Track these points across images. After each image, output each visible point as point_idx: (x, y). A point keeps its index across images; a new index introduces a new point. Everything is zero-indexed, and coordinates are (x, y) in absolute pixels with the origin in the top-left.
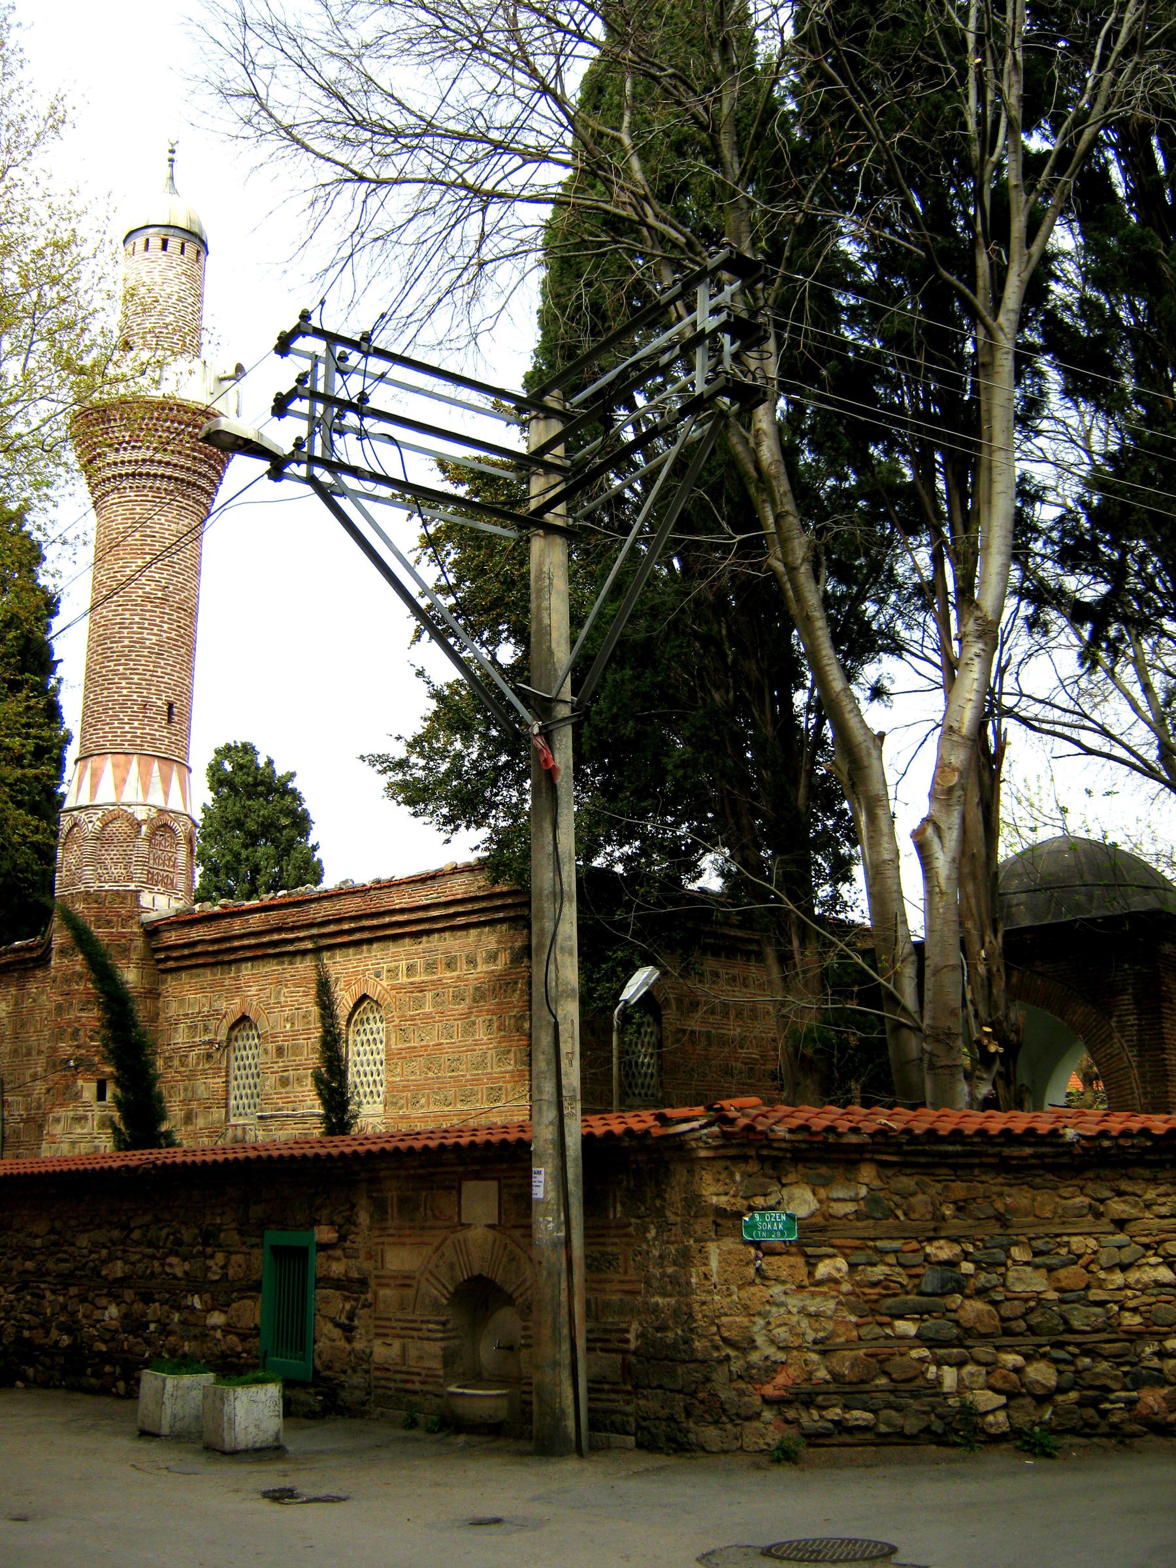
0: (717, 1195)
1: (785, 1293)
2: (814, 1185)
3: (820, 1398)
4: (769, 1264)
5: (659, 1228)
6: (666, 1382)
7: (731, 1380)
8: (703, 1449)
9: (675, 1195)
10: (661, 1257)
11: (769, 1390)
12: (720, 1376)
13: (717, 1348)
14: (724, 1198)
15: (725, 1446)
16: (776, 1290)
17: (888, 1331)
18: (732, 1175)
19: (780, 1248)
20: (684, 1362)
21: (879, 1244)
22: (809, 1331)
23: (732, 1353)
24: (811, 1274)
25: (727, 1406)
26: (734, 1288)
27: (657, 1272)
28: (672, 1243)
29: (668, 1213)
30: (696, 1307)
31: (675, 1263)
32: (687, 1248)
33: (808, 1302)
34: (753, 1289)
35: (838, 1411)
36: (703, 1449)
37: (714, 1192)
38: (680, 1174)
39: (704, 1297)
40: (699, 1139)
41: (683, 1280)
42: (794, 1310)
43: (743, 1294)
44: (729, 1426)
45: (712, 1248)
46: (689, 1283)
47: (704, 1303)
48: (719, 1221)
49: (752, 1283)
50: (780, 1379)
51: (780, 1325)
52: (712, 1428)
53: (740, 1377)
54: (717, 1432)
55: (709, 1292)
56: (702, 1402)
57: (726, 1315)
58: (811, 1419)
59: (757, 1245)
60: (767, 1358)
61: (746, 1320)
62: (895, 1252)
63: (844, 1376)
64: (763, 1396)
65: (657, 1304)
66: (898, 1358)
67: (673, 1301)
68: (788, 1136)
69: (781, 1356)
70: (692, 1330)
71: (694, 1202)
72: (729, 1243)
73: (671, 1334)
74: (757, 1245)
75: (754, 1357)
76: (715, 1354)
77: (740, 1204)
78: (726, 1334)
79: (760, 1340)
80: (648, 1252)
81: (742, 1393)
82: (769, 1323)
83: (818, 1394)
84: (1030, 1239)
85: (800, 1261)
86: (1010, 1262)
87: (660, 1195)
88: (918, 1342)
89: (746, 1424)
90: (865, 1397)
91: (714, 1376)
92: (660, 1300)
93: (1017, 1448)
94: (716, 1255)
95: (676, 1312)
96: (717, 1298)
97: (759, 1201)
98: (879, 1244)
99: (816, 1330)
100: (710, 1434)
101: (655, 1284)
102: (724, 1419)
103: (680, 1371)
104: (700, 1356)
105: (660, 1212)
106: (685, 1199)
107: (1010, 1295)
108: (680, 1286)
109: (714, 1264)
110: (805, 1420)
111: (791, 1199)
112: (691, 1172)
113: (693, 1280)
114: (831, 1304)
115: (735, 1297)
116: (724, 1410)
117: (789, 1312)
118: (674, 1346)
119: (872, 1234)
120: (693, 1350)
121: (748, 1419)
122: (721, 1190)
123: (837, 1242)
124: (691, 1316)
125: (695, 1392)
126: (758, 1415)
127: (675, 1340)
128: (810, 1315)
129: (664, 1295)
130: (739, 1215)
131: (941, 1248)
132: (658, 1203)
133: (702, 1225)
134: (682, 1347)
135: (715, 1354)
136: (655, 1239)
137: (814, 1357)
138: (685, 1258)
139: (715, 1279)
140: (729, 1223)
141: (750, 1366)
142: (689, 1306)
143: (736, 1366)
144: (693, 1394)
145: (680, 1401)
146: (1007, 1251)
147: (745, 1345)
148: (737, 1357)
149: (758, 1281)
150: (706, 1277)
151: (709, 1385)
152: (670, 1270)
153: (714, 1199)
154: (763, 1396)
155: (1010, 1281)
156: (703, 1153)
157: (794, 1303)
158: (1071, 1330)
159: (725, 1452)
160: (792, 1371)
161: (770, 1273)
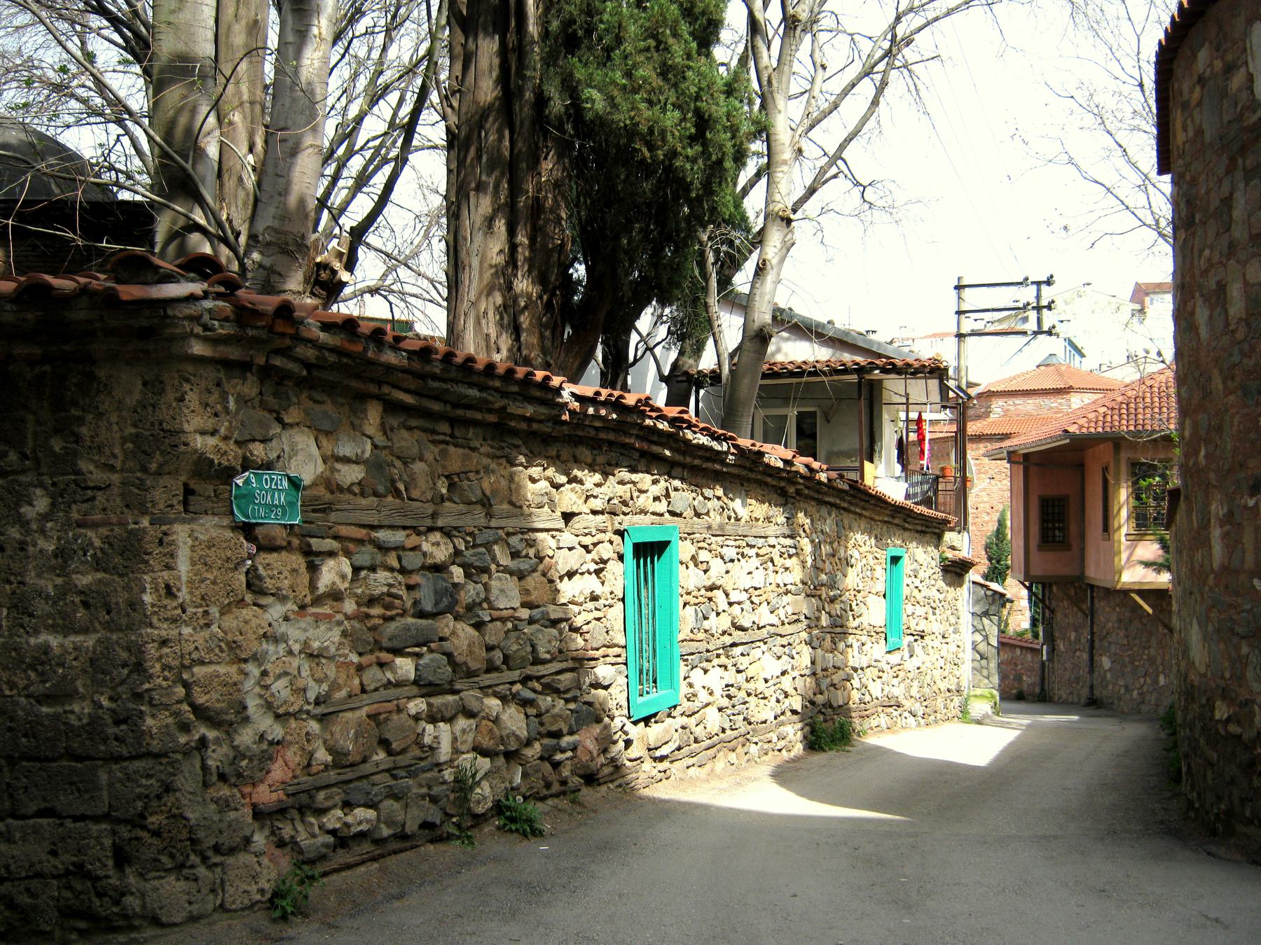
0: (203, 433)
1: (286, 619)
2: (322, 432)
3: (321, 795)
4: (267, 566)
5: (59, 497)
6: (65, 801)
7: (206, 785)
8: (156, 922)
9: (110, 429)
10: (60, 553)
11: (265, 795)
12: (187, 779)
13: (185, 728)
14: (212, 441)
15: (195, 908)
16: (276, 611)
17: (389, 675)
18: (224, 399)
19: (281, 536)
20: (119, 759)
21: (382, 535)
22: (312, 683)
23: (211, 734)
24: (313, 586)
25: (201, 834)
26: (214, 611)
27: (49, 585)
28: (94, 525)
29: (84, 465)
30: (152, 649)
31: (98, 565)
32: (137, 535)
33: (311, 633)
34: (246, 613)
35: (339, 813)
36: (156, 922)
37: (201, 431)
38: (128, 386)
39: (164, 630)
40: (196, 319)
41: (121, 598)
42: (296, 648)
43: (230, 622)
44: (202, 871)
45: (181, 533)
46: (135, 605)
47: (164, 642)
48: (193, 484)
49: (241, 603)
50: (278, 772)
51: (279, 677)
52: (172, 878)
53: (222, 777)
54: (182, 884)
55: (174, 620)
56: (156, 834)
57: (202, 663)
58: (309, 835)
59: (248, 530)
60: (262, 737)
61: (233, 669)
62: (399, 548)
63: (347, 754)
64: (254, 806)
65: (46, 649)
66: (395, 717)
67: (90, 641)
68: (323, 336)
69: (277, 732)
70: (138, 697)
71: (156, 444)
72: (211, 527)
73: (81, 709)
74: (248, 530)
75: (245, 737)
76: (183, 739)
77: (233, 454)
78: (201, 700)
79: (253, 704)
80: (22, 546)
81: (225, 805)
82: (264, 674)
83: (319, 789)
84: (508, 534)
85: (298, 561)
86: (493, 567)
87: (65, 428)
88: (415, 690)
89: (231, 860)
90: (364, 784)
91: (179, 781)
92: (54, 641)
93: (498, 828)
94: (191, 549)
95: (97, 666)
96: (186, 631)
97: (258, 450)
98: (382, 535)
99: (319, 681)
100: (170, 890)
101: (41, 607)
102: (194, 859)
103: (103, 777)
104: (156, 746)
105: (66, 463)
106: (135, 438)
107: (496, 614)
108: (115, 612)
109: (183, 566)
110: (303, 838)
111: (293, 452)
112: (154, 386)
113: (147, 598)
114: (335, 635)
115: (214, 628)
116: (194, 842)
117: (290, 653)
118: (93, 727)
119: (373, 519)
120: (140, 735)
121: (232, 851)
122: (210, 423)
123: (344, 531)
124: (139, 667)
125: (142, 816)
126: (248, 840)
127: (94, 720)
128: (311, 655)
129: (66, 627)
130: (227, 474)
131: (438, 544)
132: (57, 445)
133: (165, 492)
134: (112, 730)
135: (183, 739)
136: (45, 517)
137: (314, 726)
138: (128, 554)
139: (184, 595)
140: (209, 490)
141: (239, 754)
142: (137, 650)
143: (216, 757)
144: (138, 821)
145: (101, 838)
146: (490, 551)
147: (231, 717)
148: (217, 741)
149: (249, 598)
150: (170, 592)
151: (169, 800)
152: (84, 580)
153: (199, 442)
154: (254, 806)
155: (495, 592)
156: (198, 349)
157: (295, 634)
158: (537, 661)
159: (193, 919)
160: (293, 755)
161: (269, 584)
